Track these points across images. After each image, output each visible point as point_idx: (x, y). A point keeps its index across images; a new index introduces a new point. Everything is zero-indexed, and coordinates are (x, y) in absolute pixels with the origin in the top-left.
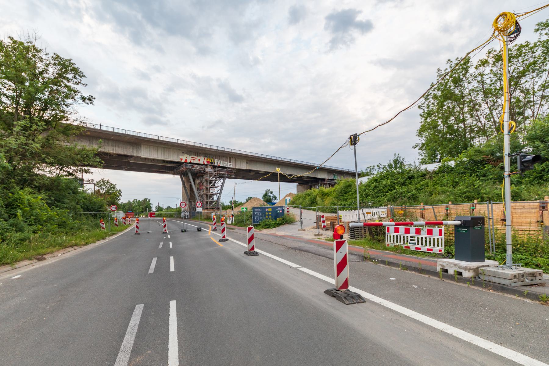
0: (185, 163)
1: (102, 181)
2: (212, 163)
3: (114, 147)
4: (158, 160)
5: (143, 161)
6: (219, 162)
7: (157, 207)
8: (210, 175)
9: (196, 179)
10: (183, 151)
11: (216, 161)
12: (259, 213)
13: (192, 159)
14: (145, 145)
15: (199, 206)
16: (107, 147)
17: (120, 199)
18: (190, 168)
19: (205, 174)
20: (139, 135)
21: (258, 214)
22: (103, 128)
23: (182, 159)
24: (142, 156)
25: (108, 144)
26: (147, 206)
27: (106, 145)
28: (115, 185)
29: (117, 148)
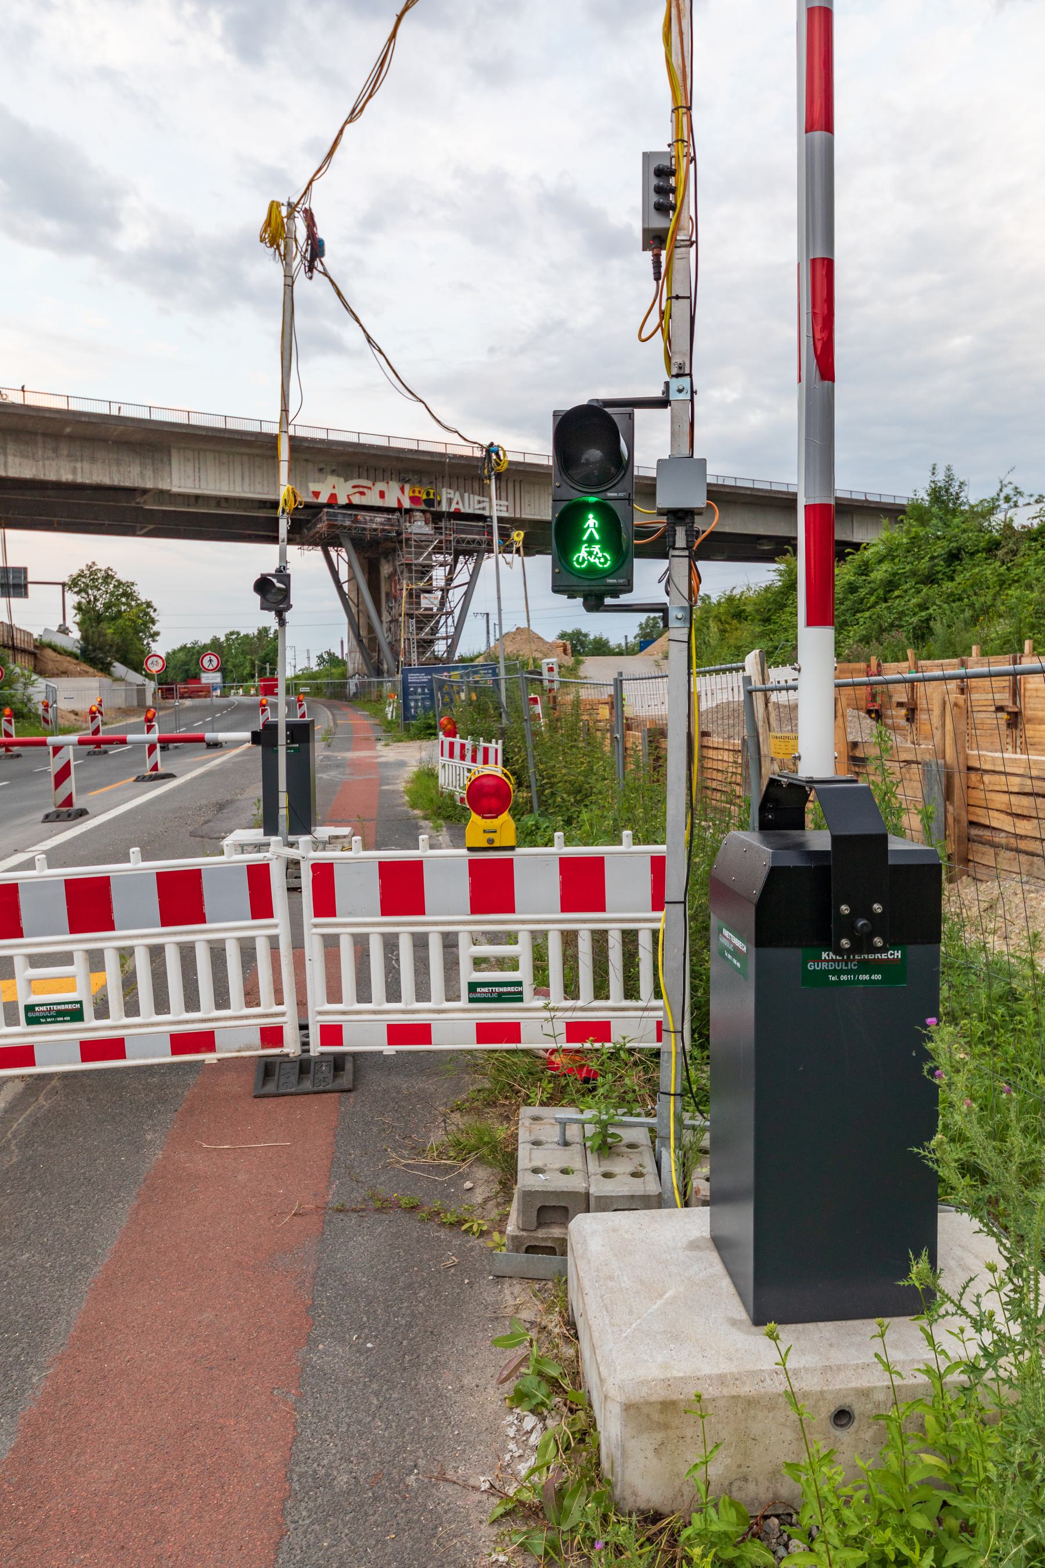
0: (329, 505)
1: (87, 572)
2: (429, 502)
3: (76, 461)
4: (227, 499)
5: (189, 505)
6: (457, 497)
7: (321, 656)
8: (421, 546)
9: (383, 561)
10: (321, 466)
11: (445, 494)
12: (423, 688)
13: (356, 490)
14: (184, 449)
15: (211, 667)
16: (54, 463)
17: (157, 634)
18: (348, 523)
19: (401, 542)
20: (158, 416)
21: (419, 690)
22: (32, 400)
23: (316, 494)
24: (175, 489)
25: (55, 450)
26: (267, 655)
27: (50, 454)
28: (133, 584)
29: (86, 465)
